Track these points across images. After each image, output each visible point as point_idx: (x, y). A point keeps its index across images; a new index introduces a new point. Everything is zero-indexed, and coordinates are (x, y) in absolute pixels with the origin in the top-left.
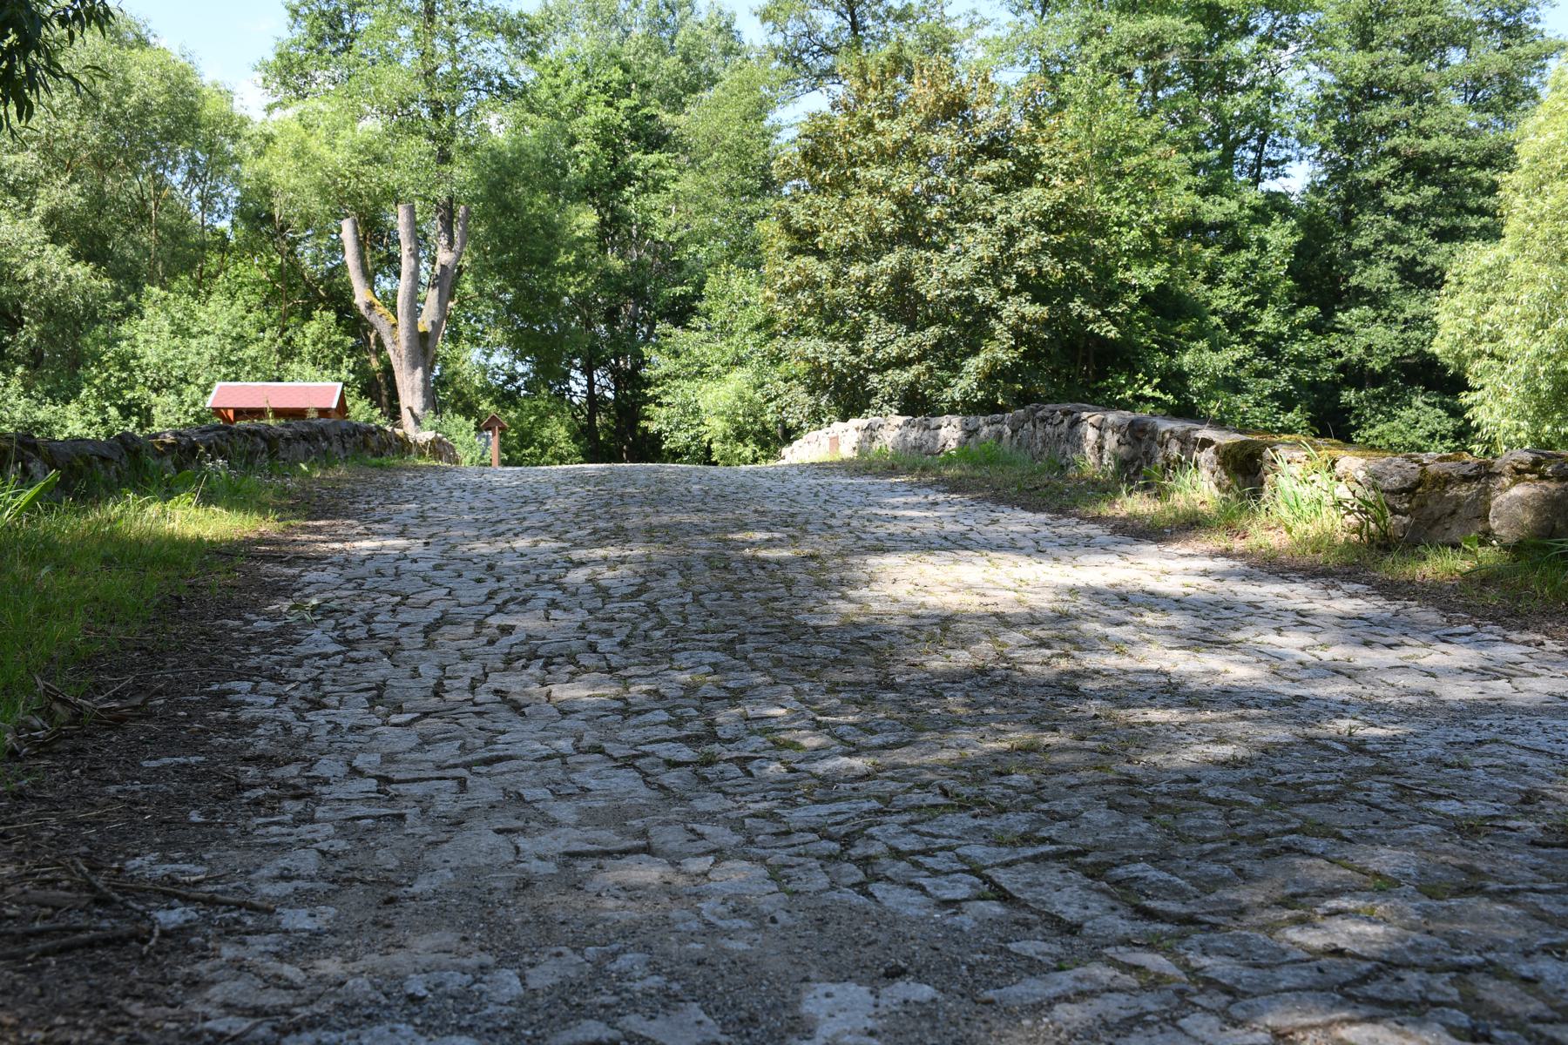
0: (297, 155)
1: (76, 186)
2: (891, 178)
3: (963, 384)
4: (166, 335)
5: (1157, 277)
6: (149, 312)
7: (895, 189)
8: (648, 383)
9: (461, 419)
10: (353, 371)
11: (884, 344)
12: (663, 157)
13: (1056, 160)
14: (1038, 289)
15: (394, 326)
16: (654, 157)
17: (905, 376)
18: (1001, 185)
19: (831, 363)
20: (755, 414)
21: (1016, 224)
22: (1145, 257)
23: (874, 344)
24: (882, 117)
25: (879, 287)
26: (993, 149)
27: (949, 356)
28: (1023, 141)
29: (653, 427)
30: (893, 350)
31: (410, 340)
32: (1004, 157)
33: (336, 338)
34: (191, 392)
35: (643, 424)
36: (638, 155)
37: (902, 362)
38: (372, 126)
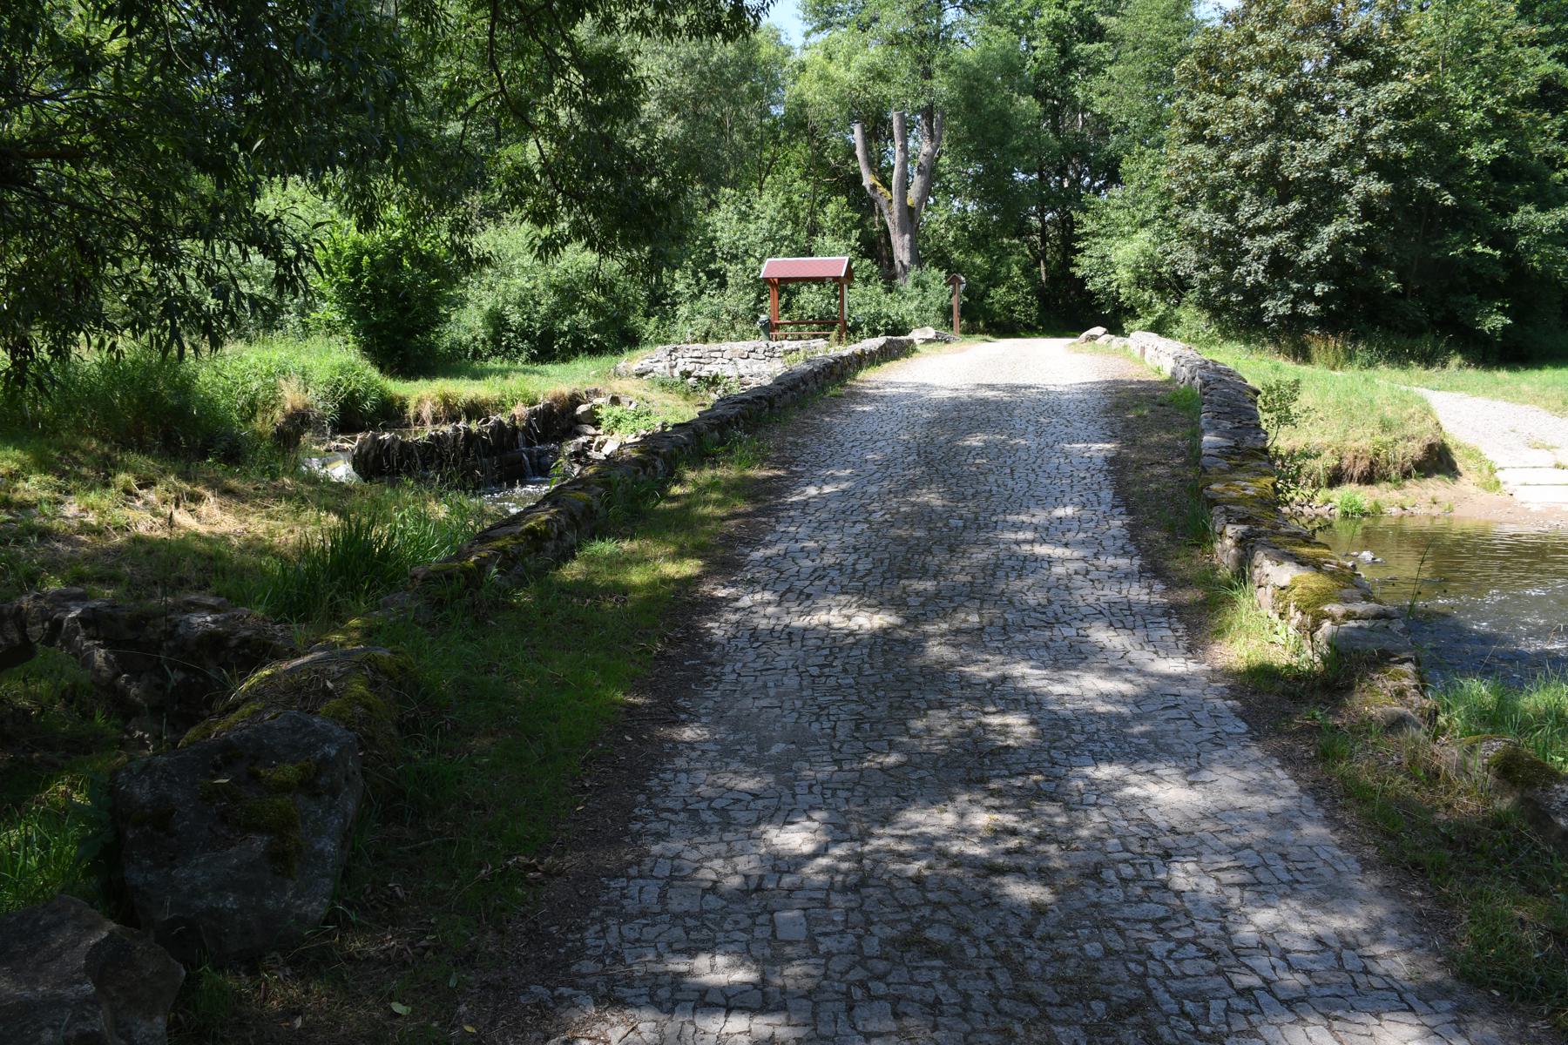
0: (820, 78)
1: (680, 122)
2: (1266, 81)
3: (1316, 248)
4: (734, 222)
5: (1494, 152)
6: (724, 206)
7: (1269, 90)
8: (1078, 238)
9: (935, 271)
10: (857, 240)
11: (1255, 215)
12: (1101, 45)
13: (1410, 57)
14: (1383, 167)
15: (891, 201)
16: (1096, 46)
17: (1268, 242)
18: (1364, 81)
19: (1211, 232)
20: (1154, 265)
21: (1370, 114)
22: (1483, 134)
23: (1247, 215)
24: (1263, 29)
25: (1253, 169)
26: (1355, 50)
27: (1303, 228)
28: (1380, 43)
29: (1079, 273)
30: (1261, 221)
31: (900, 211)
32: (1366, 58)
33: (847, 215)
34: (751, 262)
35: (1072, 270)
36: (1081, 45)
37: (1265, 230)
38: (875, 53)
